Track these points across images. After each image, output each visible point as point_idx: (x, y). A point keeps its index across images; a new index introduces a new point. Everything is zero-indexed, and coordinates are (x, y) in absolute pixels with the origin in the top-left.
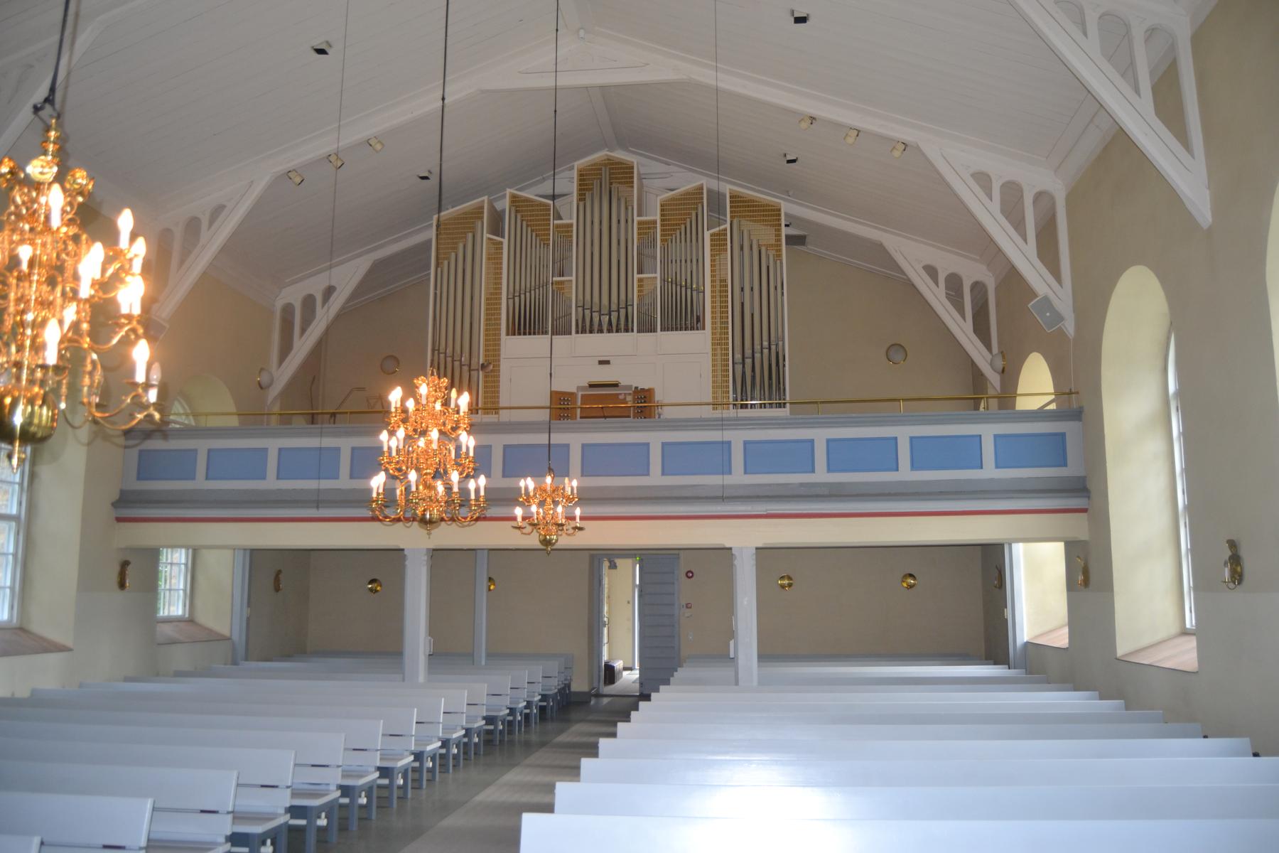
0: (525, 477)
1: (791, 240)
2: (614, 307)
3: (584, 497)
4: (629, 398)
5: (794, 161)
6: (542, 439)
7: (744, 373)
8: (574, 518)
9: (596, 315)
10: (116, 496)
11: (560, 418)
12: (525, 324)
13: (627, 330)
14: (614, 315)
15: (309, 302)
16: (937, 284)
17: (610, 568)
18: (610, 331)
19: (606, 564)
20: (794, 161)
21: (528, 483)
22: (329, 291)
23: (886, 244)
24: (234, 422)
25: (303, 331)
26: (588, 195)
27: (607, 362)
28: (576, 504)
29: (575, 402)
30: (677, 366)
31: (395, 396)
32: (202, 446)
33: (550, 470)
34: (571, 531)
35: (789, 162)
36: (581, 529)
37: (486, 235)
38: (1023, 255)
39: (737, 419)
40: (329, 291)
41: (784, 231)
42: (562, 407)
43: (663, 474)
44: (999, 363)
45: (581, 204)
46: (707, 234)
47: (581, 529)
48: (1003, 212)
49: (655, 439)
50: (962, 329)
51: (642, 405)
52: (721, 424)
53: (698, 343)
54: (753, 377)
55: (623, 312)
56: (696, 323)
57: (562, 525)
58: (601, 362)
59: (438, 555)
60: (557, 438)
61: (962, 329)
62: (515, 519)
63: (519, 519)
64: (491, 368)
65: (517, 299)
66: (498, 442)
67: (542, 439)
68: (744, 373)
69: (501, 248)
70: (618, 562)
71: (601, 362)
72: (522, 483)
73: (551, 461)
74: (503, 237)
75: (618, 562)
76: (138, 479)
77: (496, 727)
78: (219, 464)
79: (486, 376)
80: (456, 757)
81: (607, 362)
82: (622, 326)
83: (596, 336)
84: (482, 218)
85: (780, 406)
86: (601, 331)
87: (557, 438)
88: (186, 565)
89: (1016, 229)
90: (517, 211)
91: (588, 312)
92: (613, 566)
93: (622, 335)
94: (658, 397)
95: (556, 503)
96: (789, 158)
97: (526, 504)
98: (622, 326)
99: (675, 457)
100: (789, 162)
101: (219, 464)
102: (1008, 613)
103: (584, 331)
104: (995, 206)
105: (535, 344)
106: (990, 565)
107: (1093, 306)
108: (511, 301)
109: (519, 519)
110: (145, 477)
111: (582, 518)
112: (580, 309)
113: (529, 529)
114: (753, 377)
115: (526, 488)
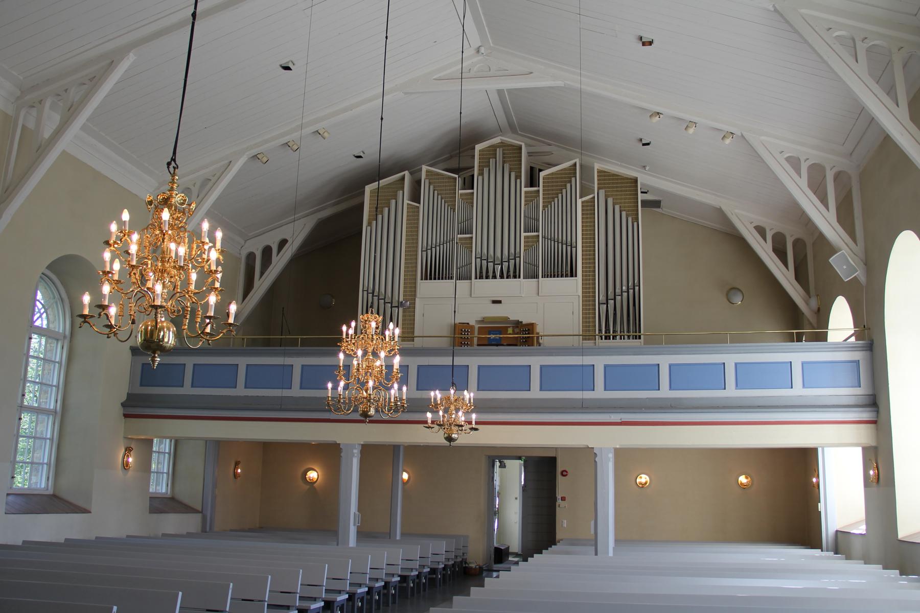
0: (435, 390)
1: (645, 204)
2: (505, 259)
3: (479, 406)
4: (510, 330)
5: (648, 144)
6: (447, 361)
7: (607, 311)
8: (470, 423)
9: (491, 265)
10: (124, 398)
11: (461, 345)
12: (435, 272)
13: (515, 277)
14: (505, 265)
15: (267, 251)
16: (765, 239)
17: (500, 467)
18: (502, 277)
19: (498, 464)
20: (648, 144)
21: (436, 395)
22: (283, 243)
23: (724, 208)
24: (577, 341)
25: (262, 274)
26: (486, 170)
27: (500, 302)
28: (472, 412)
29: (473, 333)
30: (553, 304)
31: (344, 328)
32: (189, 362)
33: (453, 384)
34: (469, 431)
35: (644, 145)
36: (476, 429)
37: (406, 202)
38: (826, 222)
39: (609, 348)
40: (283, 243)
41: (640, 197)
42: (462, 337)
43: (541, 390)
44: (814, 303)
45: (480, 178)
46: (579, 202)
47: (476, 429)
48: (810, 186)
49: (535, 362)
50: (785, 276)
51: (523, 336)
52: (582, 352)
53: (573, 287)
54: (615, 314)
55: (512, 262)
56: (573, 274)
57: (462, 426)
58: (494, 302)
59: (367, 450)
60: (459, 361)
61: (785, 276)
62: (426, 422)
63: (429, 421)
64: (410, 311)
65: (429, 252)
66: (414, 362)
67: (447, 361)
68: (607, 311)
69: (418, 212)
70: (507, 462)
71: (494, 302)
72: (432, 394)
73: (455, 378)
74: (419, 203)
75: (507, 462)
76: (141, 385)
77: (408, 584)
78: (202, 376)
79: (404, 312)
80: (378, 602)
81: (500, 302)
82: (511, 273)
83: (491, 281)
84: (403, 188)
85: (636, 337)
86: (494, 277)
87: (459, 361)
88: (169, 453)
89: (822, 202)
90: (430, 184)
91: (484, 262)
92: (503, 466)
93: (512, 280)
94: (539, 329)
95: (457, 410)
96: (644, 142)
97: (435, 411)
98: (511, 273)
99: (550, 378)
100: (644, 145)
101: (202, 376)
102: (821, 507)
103: (481, 277)
104: (804, 181)
105: (443, 287)
106: (801, 464)
107: (876, 264)
108: (424, 253)
109: (429, 421)
110: (155, 385)
111: (477, 423)
112: (478, 260)
113: (436, 427)
114: (615, 314)
115: (435, 399)
